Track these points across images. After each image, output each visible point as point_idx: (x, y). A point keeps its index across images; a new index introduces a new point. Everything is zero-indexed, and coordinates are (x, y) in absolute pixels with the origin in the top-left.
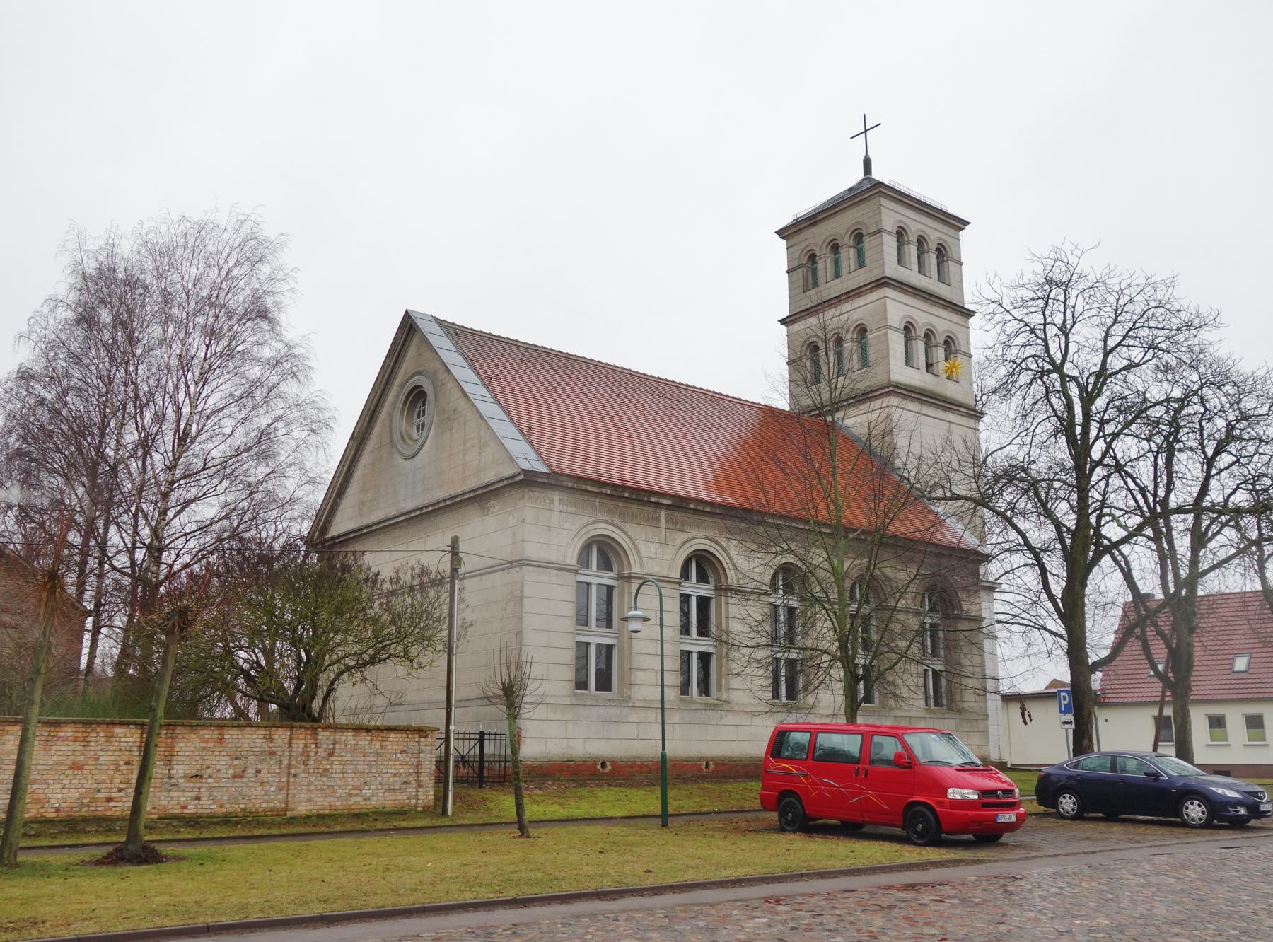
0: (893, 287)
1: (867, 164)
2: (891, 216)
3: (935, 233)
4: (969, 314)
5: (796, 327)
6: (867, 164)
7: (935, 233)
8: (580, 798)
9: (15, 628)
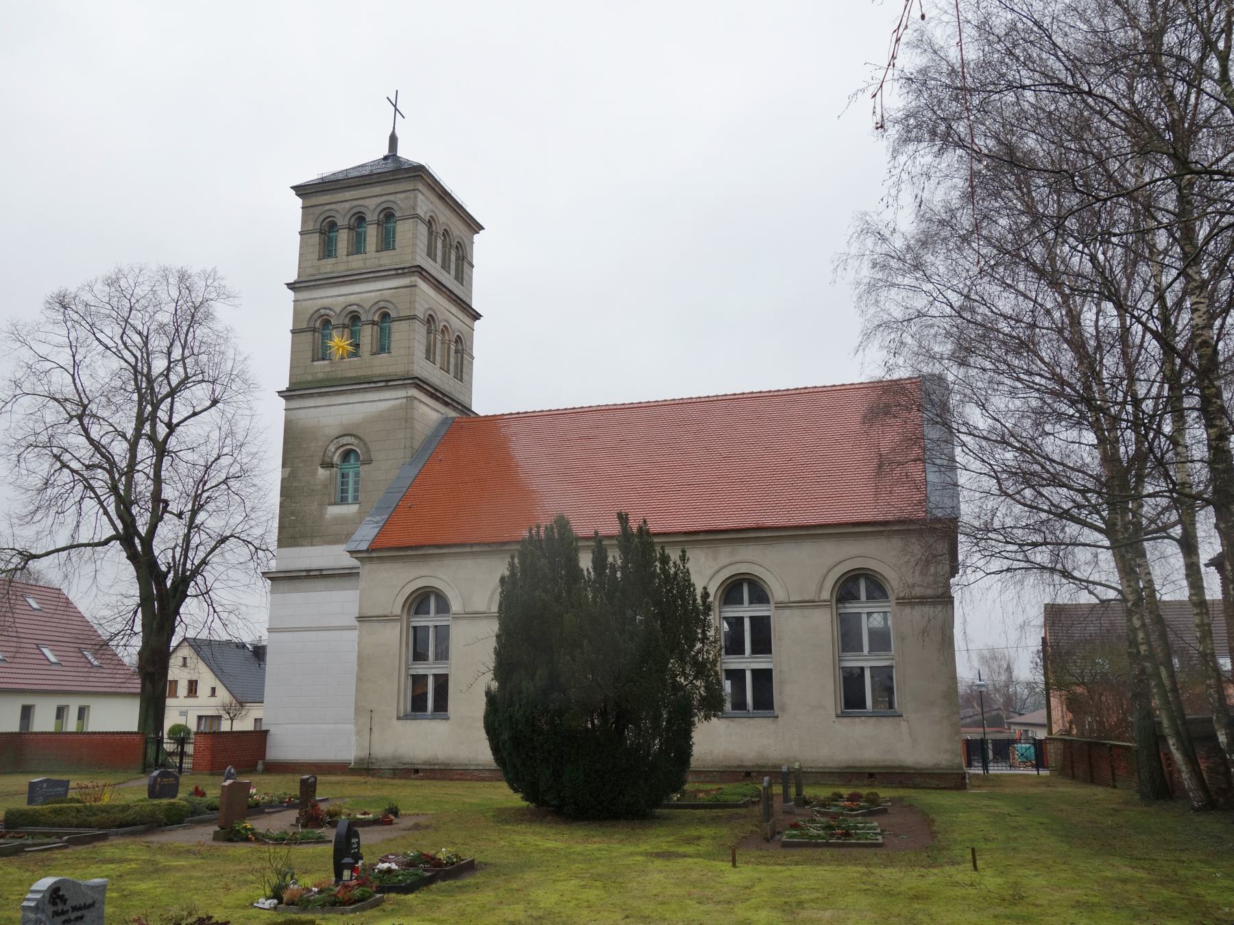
0: (424, 278)
1: (393, 140)
2: (425, 204)
3: (457, 229)
4: (476, 316)
5: (305, 295)
6: (393, 140)
7: (457, 229)
8: (658, 836)
9: (972, 885)
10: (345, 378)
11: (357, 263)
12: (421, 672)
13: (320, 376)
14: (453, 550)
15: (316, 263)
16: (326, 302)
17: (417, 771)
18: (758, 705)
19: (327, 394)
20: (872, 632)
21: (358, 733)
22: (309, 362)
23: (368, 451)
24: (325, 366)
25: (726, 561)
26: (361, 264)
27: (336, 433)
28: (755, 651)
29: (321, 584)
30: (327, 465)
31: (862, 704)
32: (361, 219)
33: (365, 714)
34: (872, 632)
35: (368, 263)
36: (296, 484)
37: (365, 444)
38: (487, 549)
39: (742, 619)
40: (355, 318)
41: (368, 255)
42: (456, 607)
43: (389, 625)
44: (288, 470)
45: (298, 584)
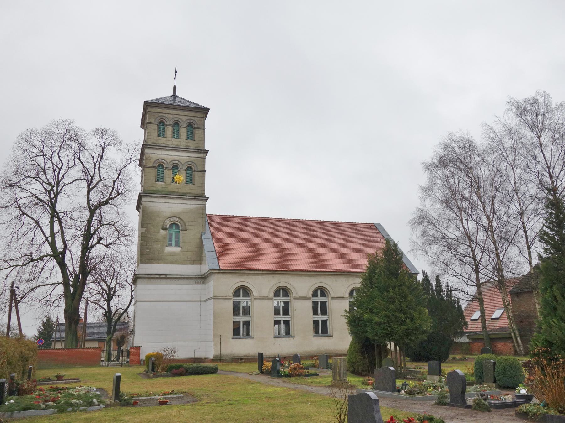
1: (175, 88)
6: (175, 88)
10: (172, 192)
11: (176, 142)
12: (238, 320)
13: (160, 189)
14: (246, 272)
15: (156, 138)
16: (163, 157)
17: (241, 359)
18: (323, 333)
19: (165, 197)
20: (243, 307)
21: (215, 345)
22: (154, 182)
23: (185, 225)
24: (162, 185)
25: (314, 282)
26: (179, 143)
27: (169, 215)
28: (322, 314)
29: (168, 281)
30: (164, 229)
31: (239, 334)
32: (176, 123)
33: (218, 337)
34: (243, 307)
35: (182, 144)
36: (149, 236)
37: (184, 222)
38: (269, 272)
39: (317, 302)
40: (161, 165)
41: (182, 140)
42: (255, 294)
43: (227, 301)
44: (144, 229)
45: (152, 280)
